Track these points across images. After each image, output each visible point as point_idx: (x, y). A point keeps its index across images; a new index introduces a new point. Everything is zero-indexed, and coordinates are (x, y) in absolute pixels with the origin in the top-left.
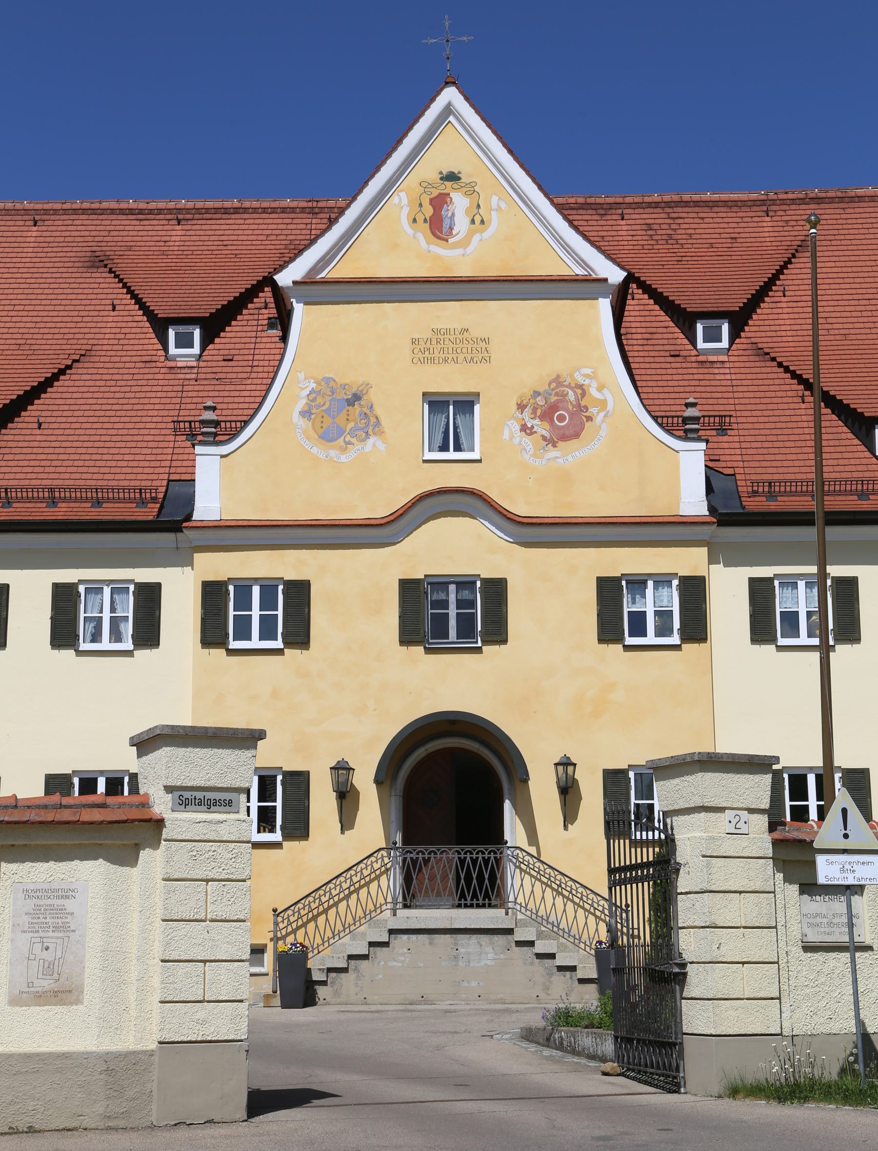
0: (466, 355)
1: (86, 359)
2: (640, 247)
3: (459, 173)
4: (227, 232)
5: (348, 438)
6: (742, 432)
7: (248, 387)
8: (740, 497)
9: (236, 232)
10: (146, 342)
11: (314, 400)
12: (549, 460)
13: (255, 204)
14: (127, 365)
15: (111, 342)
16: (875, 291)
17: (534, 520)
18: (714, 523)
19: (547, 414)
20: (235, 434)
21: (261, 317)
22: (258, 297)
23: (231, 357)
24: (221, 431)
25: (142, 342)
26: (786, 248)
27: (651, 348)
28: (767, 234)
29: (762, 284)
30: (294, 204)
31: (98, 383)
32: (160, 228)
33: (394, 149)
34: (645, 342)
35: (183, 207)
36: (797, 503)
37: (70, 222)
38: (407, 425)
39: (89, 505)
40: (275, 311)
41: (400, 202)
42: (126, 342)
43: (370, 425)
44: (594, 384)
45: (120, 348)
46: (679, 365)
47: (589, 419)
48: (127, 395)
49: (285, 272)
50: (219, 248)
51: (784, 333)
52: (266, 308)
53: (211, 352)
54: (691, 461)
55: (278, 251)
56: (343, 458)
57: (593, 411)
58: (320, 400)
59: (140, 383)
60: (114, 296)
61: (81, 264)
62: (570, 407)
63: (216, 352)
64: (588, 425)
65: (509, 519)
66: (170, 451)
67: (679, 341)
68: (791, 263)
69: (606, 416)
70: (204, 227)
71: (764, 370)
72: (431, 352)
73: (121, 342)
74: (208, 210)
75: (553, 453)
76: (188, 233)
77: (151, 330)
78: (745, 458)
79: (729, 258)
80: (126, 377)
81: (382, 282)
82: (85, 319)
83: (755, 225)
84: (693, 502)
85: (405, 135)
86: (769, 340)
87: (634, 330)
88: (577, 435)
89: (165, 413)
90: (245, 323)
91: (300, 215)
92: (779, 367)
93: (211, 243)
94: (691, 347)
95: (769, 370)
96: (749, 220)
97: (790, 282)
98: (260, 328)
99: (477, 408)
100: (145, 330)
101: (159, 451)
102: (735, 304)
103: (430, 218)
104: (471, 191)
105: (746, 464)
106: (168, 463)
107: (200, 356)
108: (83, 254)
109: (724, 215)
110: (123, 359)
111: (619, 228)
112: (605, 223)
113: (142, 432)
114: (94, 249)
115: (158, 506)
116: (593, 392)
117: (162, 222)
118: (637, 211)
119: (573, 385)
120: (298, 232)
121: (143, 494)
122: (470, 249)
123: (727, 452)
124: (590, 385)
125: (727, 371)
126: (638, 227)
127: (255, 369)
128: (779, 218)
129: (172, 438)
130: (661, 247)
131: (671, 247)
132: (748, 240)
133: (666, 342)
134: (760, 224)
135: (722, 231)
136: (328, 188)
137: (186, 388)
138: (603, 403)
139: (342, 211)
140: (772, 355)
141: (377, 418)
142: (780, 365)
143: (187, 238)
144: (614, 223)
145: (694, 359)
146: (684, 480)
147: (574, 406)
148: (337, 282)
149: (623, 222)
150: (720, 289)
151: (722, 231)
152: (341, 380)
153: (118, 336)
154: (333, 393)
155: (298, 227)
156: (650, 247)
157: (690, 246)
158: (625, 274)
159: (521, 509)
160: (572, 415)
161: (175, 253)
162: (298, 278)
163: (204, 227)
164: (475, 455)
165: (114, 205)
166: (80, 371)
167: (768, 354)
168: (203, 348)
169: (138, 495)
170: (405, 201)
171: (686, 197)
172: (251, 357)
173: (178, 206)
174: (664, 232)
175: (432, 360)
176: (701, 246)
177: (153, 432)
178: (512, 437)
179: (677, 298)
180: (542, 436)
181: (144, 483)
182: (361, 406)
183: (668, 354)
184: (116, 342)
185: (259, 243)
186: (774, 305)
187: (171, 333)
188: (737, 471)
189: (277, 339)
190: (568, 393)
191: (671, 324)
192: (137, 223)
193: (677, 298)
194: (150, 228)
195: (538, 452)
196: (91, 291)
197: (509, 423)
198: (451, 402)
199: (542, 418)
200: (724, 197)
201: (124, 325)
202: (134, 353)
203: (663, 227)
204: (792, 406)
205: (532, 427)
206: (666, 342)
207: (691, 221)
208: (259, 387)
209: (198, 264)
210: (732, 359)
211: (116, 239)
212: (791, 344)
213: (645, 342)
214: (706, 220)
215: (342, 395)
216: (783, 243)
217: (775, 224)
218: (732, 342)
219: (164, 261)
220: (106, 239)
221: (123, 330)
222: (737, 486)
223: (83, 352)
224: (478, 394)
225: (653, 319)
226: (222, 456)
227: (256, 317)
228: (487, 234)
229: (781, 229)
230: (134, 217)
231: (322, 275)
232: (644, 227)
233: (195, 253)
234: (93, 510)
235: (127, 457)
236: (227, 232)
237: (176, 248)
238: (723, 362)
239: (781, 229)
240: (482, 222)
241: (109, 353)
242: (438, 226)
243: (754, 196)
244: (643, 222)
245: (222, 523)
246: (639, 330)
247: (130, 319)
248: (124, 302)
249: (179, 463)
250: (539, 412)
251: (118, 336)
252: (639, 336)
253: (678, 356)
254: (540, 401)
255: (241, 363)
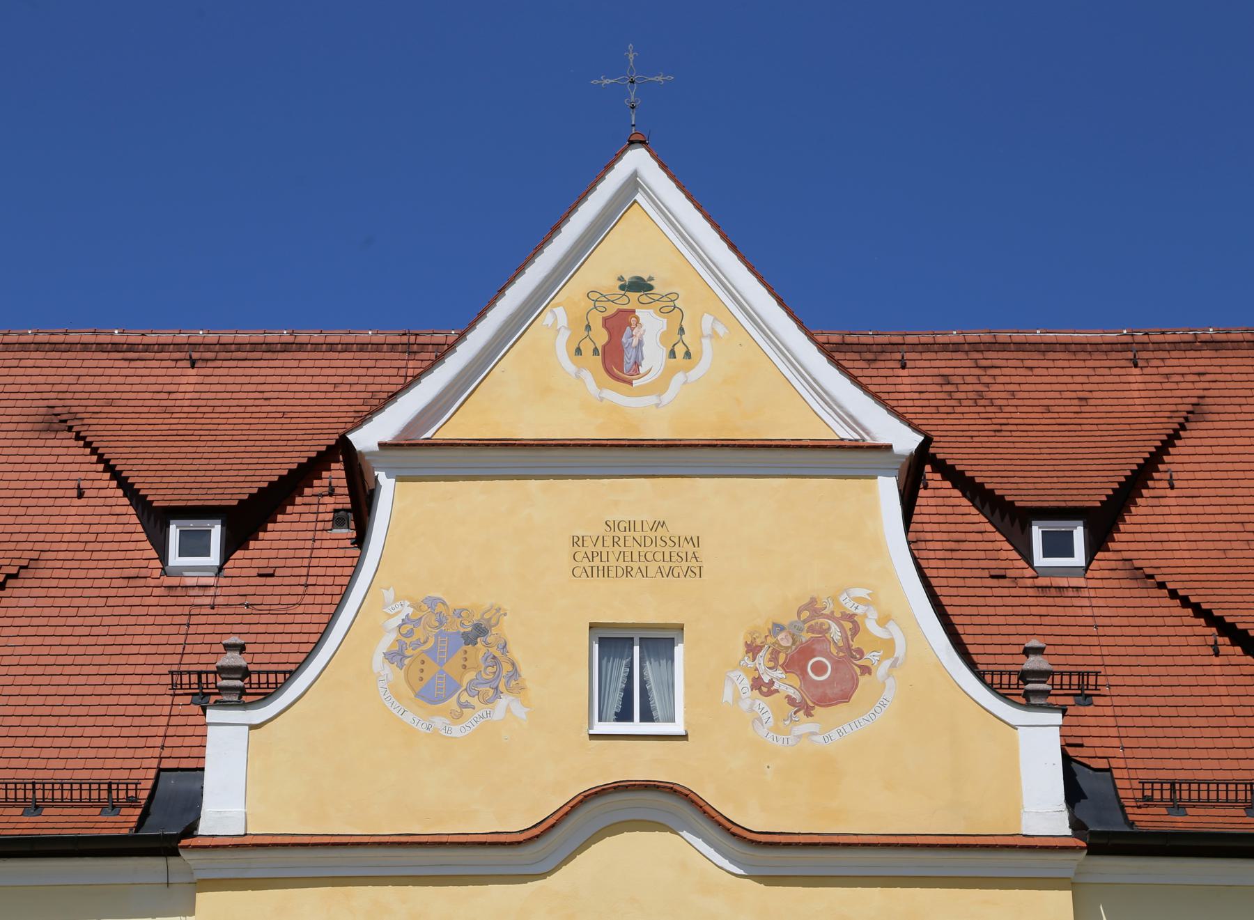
0: (661, 564)
1: (30, 573)
2: (934, 410)
3: (651, 279)
4: (270, 380)
5: (465, 698)
6: (1116, 701)
7: (299, 619)
8: (1122, 807)
9: (285, 380)
10: (132, 546)
11: (410, 634)
12: (800, 737)
13: (317, 338)
14: (98, 583)
15: (73, 546)
16: (1248, 680)
17: (777, 839)
18: (1082, 848)
19: (796, 661)
20: (271, 694)
21: (322, 508)
22: (321, 478)
23: (271, 571)
24: (251, 686)
25: (124, 546)
26: (1168, 414)
27: (958, 564)
28: (1136, 394)
29: (1135, 467)
30: (379, 339)
31: (47, 612)
32: (163, 372)
33: (547, 240)
34: (948, 554)
35: (199, 340)
36: (1220, 820)
37: (15, 363)
38: (563, 675)
39: (20, 811)
40: (348, 500)
41: (556, 320)
42: (98, 546)
43: (502, 676)
44: (873, 615)
45: (87, 555)
46: (1005, 592)
47: (866, 670)
48: (95, 631)
49: (367, 428)
50: (257, 403)
51: (1175, 546)
52: (331, 495)
53: (238, 563)
54: (1038, 741)
55: (353, 409)
56: (456, 731)
57: (871, 657)
58: (419, 634)
59: (117, 611)
60: (82, 475)
61: (29, 427)
62: (834, 651)
63: (246, 563)
64: (863, 680)
65: (734, 834)
66: (164, 721)
67: (1003, 555)
68: (1180, 438)
69: (893, 666)
70: (233, 372)
71: (1146, 602)
72: (604, 558)
73: (90, 547)
74: (240, 346)
75: (806, 726)
76: (208, 380)
77: (140, 528)
78: (1126, 743)
79: (1079, 428)
80: (94, 602)
81: (525, 445)
82: (31, 511)
83: (1117, 379)
84: (1044, 811)
85: (565, 218)
86: (1152, 555)
87: (929, 536)
88: (845, 697)
89: (159, 659)
90: (295, 517)
91: (388, 355)
92: (1172, 598)
93: (244, 395)
94: (1023, 564)
95: (1155, 602)
96: (1106, 371)
97: (1179, 467)
98: (320, 526)
99: (679, 650)
100: (131, 528)
101: (146, 721)
102: (1095, 494)
103: (604, 347)
104: (669, 307)
105: (1128, 753)
106: (159, 742)
107: (221, 568)
108: (33, 411)
109: (1066, 364)
110: (92, 574)
111: (898, 380)
112: (874, 372)
113: (117, 690)
114: (52, 403)
115: (138, 811)
116: (872, 626)
117: (165, 364)
118: (925, 356)
119: (838, 615)
120: (385, 380)
121: (114, 793)
122: (667, 397)
123: (1095, 731)
124: (865, 616)
125: (1086, 602)
126: (929, 380)
127: (311, 590)
128: (1154, 371)
129: (168, 700)
130: (966, 410)
131: (982, 409)
132: (1105, 402)
133: (981, 555)
134: (1124, 379)
135: (1063, 387)
136: (437, 303)
137: (194, 620)
138: (889, 645)
139: (452, 347)
140: (1159, 579)
141: (513, 664)
142: (1173, 594)
143: (206, 388)
144: (890, 372)
145: (1029, 582)
146: (1025, 773)
147: (839, 649)
148: (452, 445)
149: (905, 372)
150: (1067, 474)
151: (1063, 387)
152: (454, 602)
153: (84, 538)
154: (441, 623)
155: (388, 369)
156: (950, 410)
157: (1013, 409)
158: (921, 438)
159: (753, 819)
160: (836, 663)
161: (186, 409)
162: (388, 437)
163: (233, 372)
164: (677, 728)
165: (88, 338)
166: (17, 592)
167: (1151, 577)
168: (226, 555)
169: (104, 795)
170: (563, 321)
171: (1003, 337)
172: (304, 571)
173: (193, 340)
174: (970, 388)
175: (605, 572)
176: (1030, 409)
177: (135, 690)
178: (737, 698)
179: (998, 486)
180: (788, 697)
181: (116, 775)
182: (487, 644)
183: (986, 573)
184: (81, 546)
185: (323, 395)
186: (1155, 502)
187: (174, 531)
188: (1114, 763)
189: (348, 543)
190: (829, 628)
191: (989, 527)
192: (125, 364)
193: (998, 486)
194: (146, 372)
195: (781, 725)
196: (43, 467)
197: (732, 675)
198: (636, 641)
199: (787, 667)
200: (1063, 337)
201: (96, 519)
202: (110, 564)
203: (968, 379)
204: (1198, 660)
205: (772, 682)
206: (981, 555)
207: (1013, 371)
208: (316, 619)
209: (221, 427)
210: (1092, 583)
211: (88, 388)
212: (1188, 563)
213: (948, 554)
214: (1036, 371)
215: (455, 627)
216: (1164, 408)
217: (1148, 378)
218: (1090, 557)
219: (166, 421)
220: (72, 388)
221: (94, 529)
222: (1116, 789)
223: (25, 563)
224: (680, 628)
225: (960, 519)
226: (253, 727)
227: (314, 508)
228: (695, 374)
229: (1158, 386)
230: (120, 355)
231: (428, 435)
232: (939, 380)
233: (217, 409)
234: (26, 819)
235: (88, 732)
236: (270, 380)
237: (187, 403)
238: (1078, 588)
239: (1158, 386)
240: (688, 354)
241: (68, 564)
242: (616, 360)
243: (1111, 337)
244: (936, 372)
245: (248, 840)
246: (937, 536)
247: (107, 510)
248: (97, 484)
249: (178, 741)
250: (782, 658)
251: (84, 538)
252: (938, 545)
253: (1004, 577)
254: (784, 639)
255: (287, 581)
